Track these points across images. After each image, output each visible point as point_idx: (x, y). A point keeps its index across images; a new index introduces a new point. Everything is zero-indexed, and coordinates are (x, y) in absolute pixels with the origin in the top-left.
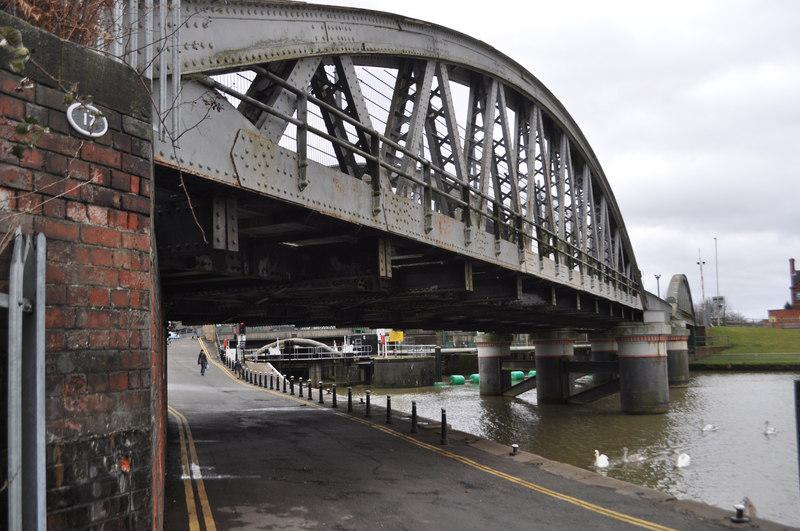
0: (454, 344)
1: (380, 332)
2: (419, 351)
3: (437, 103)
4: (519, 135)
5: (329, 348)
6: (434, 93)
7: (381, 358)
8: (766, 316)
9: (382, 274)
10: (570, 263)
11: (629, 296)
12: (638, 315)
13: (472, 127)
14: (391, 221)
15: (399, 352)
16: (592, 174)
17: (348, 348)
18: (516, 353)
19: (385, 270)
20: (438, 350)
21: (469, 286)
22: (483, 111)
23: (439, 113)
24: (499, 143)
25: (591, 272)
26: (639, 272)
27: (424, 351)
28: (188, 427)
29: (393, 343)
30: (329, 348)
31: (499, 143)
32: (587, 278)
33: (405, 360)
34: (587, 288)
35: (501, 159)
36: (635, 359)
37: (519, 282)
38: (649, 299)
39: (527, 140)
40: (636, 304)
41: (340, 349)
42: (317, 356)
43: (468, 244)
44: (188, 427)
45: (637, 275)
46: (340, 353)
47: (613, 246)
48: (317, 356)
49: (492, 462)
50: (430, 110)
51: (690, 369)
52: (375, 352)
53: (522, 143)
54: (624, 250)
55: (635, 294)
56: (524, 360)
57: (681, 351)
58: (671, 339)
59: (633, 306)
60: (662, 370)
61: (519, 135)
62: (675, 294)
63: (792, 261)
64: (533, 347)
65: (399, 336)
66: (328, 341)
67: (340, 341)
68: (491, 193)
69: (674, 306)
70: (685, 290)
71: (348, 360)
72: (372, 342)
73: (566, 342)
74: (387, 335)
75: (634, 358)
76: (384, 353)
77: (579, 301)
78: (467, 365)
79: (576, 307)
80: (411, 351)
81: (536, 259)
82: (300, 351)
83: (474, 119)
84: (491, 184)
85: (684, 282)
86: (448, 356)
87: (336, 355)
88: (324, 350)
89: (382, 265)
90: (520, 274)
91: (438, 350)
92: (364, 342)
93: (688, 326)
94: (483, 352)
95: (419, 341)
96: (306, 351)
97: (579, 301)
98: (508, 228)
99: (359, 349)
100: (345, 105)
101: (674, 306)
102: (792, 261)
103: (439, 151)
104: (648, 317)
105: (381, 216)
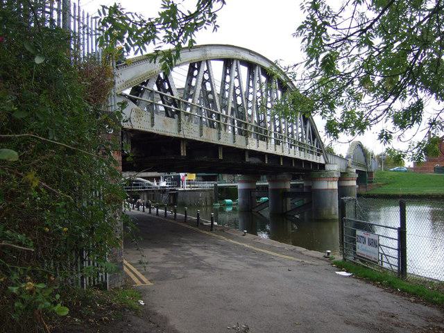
0: (226, 182)
1: (182, 175)
2: (204, 185)
3: (206, 77)
4: (249, 80)
5: (152, 183)
6: (205, 72)
7: (182, 189)
9: (182, 154)
12: (322, 166)
13: (224, 82)
14: (186, 133)
15: (193, 186)
17: (163, 184)
18: (258, 187)
19: (183, 153)
20: (216, 185)
21: (221, 157)
22: (253, 80)
23: (207, 81)
27: (208, 185)
29: (190, 180)
30: (152, 183)
33: (194, 191)
34: (297, 156)
36: (319, 190)
37: (266, 156)
40: (321, 160)
41: (158, 184)
42: (145, 188)
43: (179, 131)
46: (158, 186)
48: (145, 188)
49: (229, 236)
50: (204, 79)
52: (179, 186)
53: (251, 85)
55: (319, 155)
57: (333, 190)
59: (318, 161)
61: (249, 80)
64: (267, 184)
65: (193, 177)
66: (151, 179)
67: (158, 179)
69: (350, 160)
71: (163, 190)
72: (178, 180)
73: (284, 181)
74: (186, 175)
76: (185, 187)
77: (266, 158)
79: (280, 163)
80: (200, 185)
82: (135, 185)
83: (225, 78)
86: (222, 189)
87: (156, 188)
88: (149, 185)
89: (182, 151)
90: (246, 150)
91: (216, 185)
92: (172, 180)
93: (357, 171)
94: (240, 186)
95: (205, 179)
96: (138, 185)
97: (266, 158)
99: (169, 184)
100: (167, 87)
105: (181, 132)
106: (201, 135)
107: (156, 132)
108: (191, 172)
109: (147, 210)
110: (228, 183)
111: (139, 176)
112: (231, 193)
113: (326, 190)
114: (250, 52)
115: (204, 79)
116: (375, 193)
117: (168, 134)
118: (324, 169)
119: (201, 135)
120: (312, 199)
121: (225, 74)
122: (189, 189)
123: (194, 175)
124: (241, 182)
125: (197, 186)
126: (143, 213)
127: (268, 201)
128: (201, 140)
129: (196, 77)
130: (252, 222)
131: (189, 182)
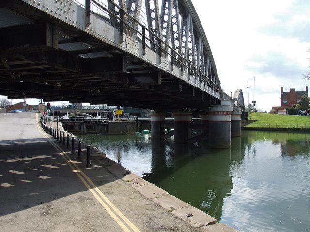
8: (272, 109)
10: (201, 81)
11: (213, 91)
12: (218, 102)
16: (194, 22)
24: (174, 17)
25: (208, 85)
26: (220, 81)
28: (88, 186)
31: (174, 17)
32: (207, 87)
35: (175, 23)
38: (224, 96)
39: (169, 5)
40: (217, 96)
44: (88, 186)
45: (218, 82)
47: (206, 68)
51: (242, 130)
54: (211, 66)
56: (170, 124)
58: (233, 114)
60: (229, 127)
62: (237, 97)
63: (282, 88)
68: (170, 44)
70: (241, 96)
75: (215, 122)
78: (145, 124)
81: (187, 76)
83: (165, 5)
84: (170, 39)
85: (241, 93)
98: (178, 62)
101: (236, 102)
102: (282, 88)
103: (173, 36)
104: (223, 103)
113: (220, 122)
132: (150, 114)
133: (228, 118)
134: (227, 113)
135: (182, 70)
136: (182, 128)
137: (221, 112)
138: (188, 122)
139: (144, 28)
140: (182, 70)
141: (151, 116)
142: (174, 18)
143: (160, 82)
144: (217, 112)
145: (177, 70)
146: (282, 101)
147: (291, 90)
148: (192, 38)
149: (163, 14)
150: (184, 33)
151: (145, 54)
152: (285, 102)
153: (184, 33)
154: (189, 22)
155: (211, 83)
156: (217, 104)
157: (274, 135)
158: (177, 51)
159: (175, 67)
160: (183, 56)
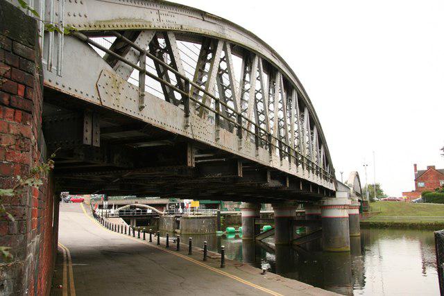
0: (229, 208)
6: (222, 60)
9: (189, 165)
12: (332, 194)
14: (196, 133)
20: (219, 212)
21: (240, 174)
23: (224, 71)
25: (308, 168)
27: (211, 213)
29: (193, 208)
34: (306, 178)
40: (331, 187)
50: (220, 69)
53: (271, 92)
56: (267, 218)
60: (345, 225)
63: (415, 165)
65: (196, 204)
70: (357, 180)
77: (288, 181)
83: (244, 77)
95: (208, 206)
97: (288, 181)
98: (263, 140)
101: (352, 189)
102: (415, 165)
104: (338, 194)
106: (217, 139)
107: (146, 120)
108: (195, 198)
109: (154, 238)
110: (230, 210)
111: (145, 202)
112: (235, 221)
113: (337, 218)
114: (272, 51)
115: (220, 69)
116: (368, 221)
117: (168, 129)
118: (335, 197)
119: (217, 139)
120: (322, 227)
121: (245, 72)
122: (193, 216)
123: (198, 202)
124: (245, 209)
125: (199, 213)
126: (149, 244)
127: (273, 229)
128: (218, 147)
129: (209, 61)
130: (255, 254)
131: (193, 209)
132: (241, 207)
133: (344, 213)
134: (344, 207)
135: (270, 152)
136: (285, 225)
137: (336, 206)
138: (292, 217)
139: (217, 101)
140: (270, 152)
141: (241, 210)
142: (259, 99)
143: (240, 174)
144: (332, 206)
145: (186, 67)
146: (416, 184)
147: (429, 167)
148: (283, 103)
149: (243, 91)
150: (271, 100)
151: (143, 107)
152: (421, 184)
153: (271, 100)
154: (279, 81)
155: (326, 173)
156: (331, 197)
157: (418, 233)
158: (262, 126)
159: (223, 131)
160: (272, 132)
